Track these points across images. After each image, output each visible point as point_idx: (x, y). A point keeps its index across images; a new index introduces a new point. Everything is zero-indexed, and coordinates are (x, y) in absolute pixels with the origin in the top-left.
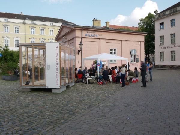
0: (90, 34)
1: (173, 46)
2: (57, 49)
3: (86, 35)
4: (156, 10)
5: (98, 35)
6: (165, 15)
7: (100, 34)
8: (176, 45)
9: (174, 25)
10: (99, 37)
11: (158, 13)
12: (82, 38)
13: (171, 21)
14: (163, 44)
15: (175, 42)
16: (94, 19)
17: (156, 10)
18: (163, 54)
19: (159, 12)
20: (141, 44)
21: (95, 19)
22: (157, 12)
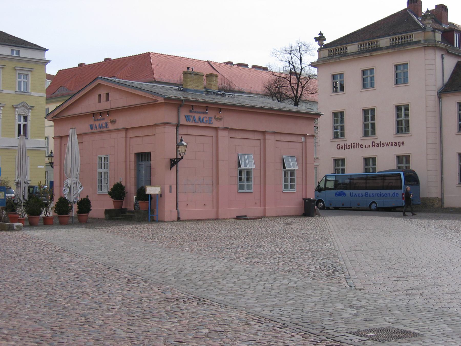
0: (197, 116)
1: (370, 143)
2: (394, 195)
3: (187, 118)
4: (321, 34)
5: (213, 118)
6: (346, 54)
7: (218, 116)
8: (377, 142)
9: (372, 85)
10: (216, 124)
11: (325, 43)
12: (178, 126)
13: (364, 72)
14: (343, 135)
15: (374, 133)
16: (188, 68)
17: (321, 34)
18: (343, 164)
19: (329, 39)
20: (306, 142)
21: (190, 70)
22: (325, 40)
